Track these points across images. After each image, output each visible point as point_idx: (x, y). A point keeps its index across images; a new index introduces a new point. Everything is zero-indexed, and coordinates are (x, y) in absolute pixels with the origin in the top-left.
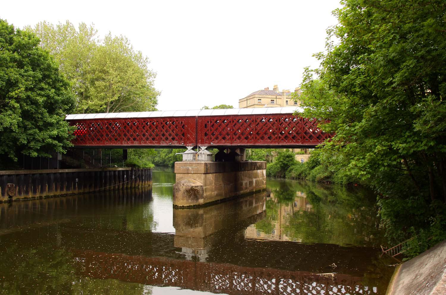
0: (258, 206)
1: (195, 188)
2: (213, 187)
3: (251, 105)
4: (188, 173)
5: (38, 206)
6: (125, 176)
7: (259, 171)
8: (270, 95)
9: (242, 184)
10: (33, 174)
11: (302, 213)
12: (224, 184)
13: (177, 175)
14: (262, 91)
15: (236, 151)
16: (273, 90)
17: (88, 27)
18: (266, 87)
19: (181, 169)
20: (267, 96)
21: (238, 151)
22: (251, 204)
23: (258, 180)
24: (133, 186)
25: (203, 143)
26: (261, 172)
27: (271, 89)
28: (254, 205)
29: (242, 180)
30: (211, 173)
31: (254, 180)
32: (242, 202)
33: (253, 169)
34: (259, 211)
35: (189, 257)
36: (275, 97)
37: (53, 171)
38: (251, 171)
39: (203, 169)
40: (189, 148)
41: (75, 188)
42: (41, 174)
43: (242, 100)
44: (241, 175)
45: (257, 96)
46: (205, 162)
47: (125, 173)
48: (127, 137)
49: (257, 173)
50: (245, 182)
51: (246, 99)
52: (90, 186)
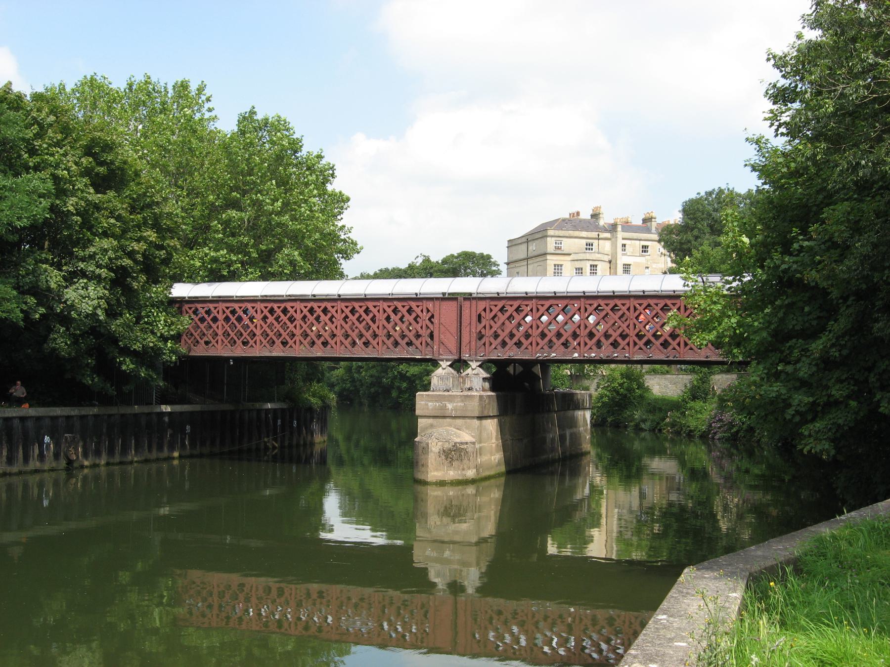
1: (462, 447)
2: (494, 445)
3: (536, 253)
4: (444, 417)
6: (295, 425)
7: (579, 413)
9: (544, 440)
10: (110, 416)
11: (694, 486)
12: (512, 440)
13: (419, 420)
14: (564, 220)
15: (533, 369)
17: (193, 87)
18: (574, 210)
19: (430, 408)
20: (577, 233)
21: (537, 370)
24: (295, 442)
27: (586, 215)
36: (595, 234)
37: (146, 409)
42: (123, 415)
45: (550, 232)
46: (478, 394)
48: (309, 338)
51: (524, 240)
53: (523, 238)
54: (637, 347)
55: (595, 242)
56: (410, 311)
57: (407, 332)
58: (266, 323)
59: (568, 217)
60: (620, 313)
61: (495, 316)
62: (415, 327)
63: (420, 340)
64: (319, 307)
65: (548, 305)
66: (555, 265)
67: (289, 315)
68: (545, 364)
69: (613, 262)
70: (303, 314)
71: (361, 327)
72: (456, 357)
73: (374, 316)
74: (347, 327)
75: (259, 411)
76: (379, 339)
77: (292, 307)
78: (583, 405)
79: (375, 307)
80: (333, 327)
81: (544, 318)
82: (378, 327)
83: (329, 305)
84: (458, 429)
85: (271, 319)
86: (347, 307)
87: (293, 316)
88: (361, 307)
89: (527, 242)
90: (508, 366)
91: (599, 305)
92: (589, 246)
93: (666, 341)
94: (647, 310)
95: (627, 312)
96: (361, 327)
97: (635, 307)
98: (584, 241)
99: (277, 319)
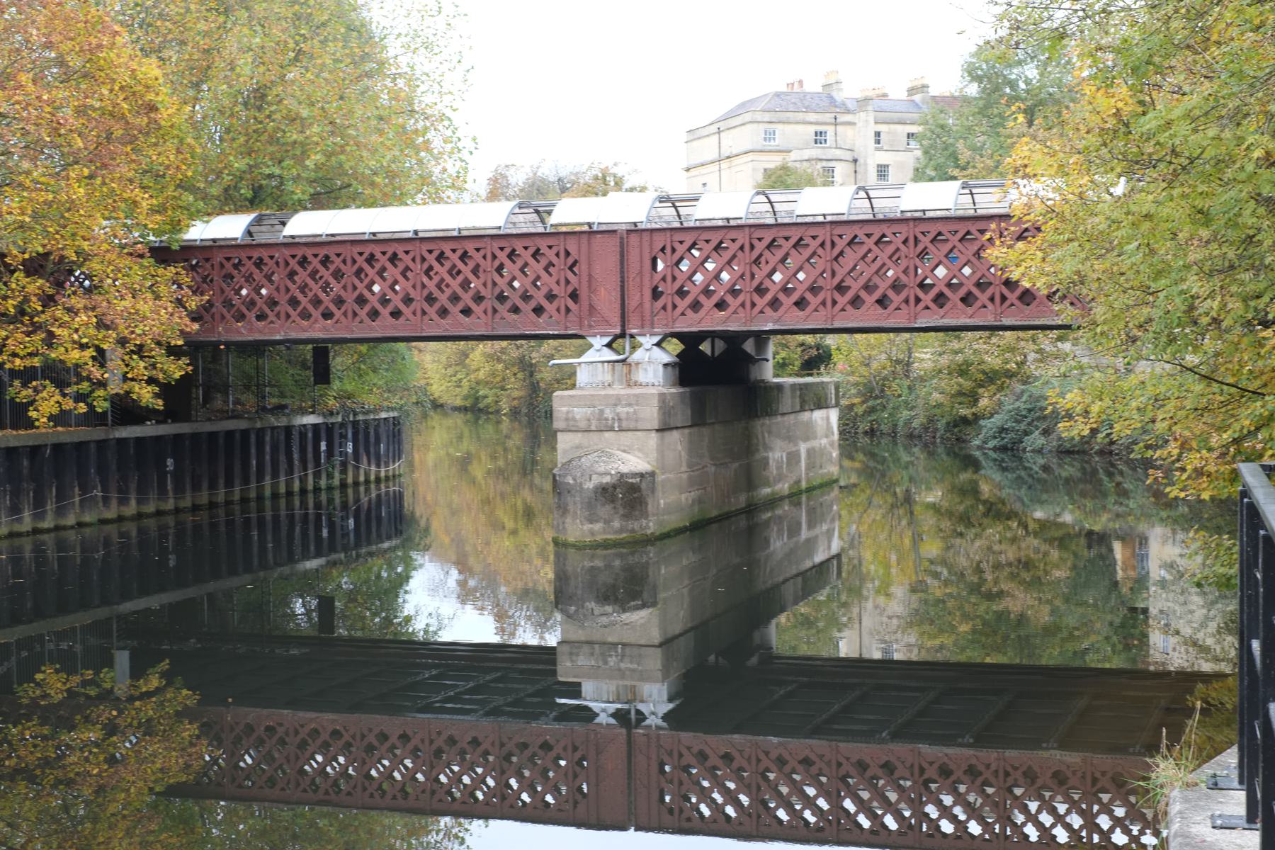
0: (816, 537)
5: (52, 554)
7: (818, 415)
8: (808, 110)
13: (560, 436)
14: (778, 95)
16: (820, 90)
20: (800, 116)
21: (749, 346)
22: (794, 530)
23: (813, 449)
25: (647, 325)
26: (822, 418)
28: (805, 534)
29: (767, 448)
30: (677, 428)
31: (803, 448)
32: (767, 523)
33: (798, 408)
34: (819, 557)
35: (603, 710)
36: (828, 117)
38: (792, 416)
39: (656, 415)
40: (598, 342)
41: (162, 491)
43: (698, 134)
44: (763, 433)
47: (323, 435)
49: (809, 425)
50: (776, 454)
51: (714, 128)
52: (142, 491)
53: (712, 127)
54: (922, 305)
55: (830, 130)
56: (536, 254)
57: (532, 291)
58: (294, 282)
59: (784, 89)
60: (891, 249)
61: (841, 254)
62: (547, 282)
63: (556, 303)
64: (316, 256)
65: (797, 238)
66: (765, 170)
67: (310, 269)
68: (761, 338)
69: (861, 161)
70: (356, 267)
71: (455, 284)
72: (618, 331)
73: (478, 266)
74: (431, 285)
75: (288, 429)
76: (487, 304)
77: (338, 255)
78: (826, 402)
79: (478, 250)
80: (409, 285)
81: (685, 266)
82: (485, 285)
83: (400, 250)
84: (624, 451)
85: (302, 276)
86: (430, 252)
87: (340, 270)
88: (526, 248)
89: (719, 131)
90: (700, 343)
91: (968, 233)
92: (819, 138)
93: (969, 293)
94: (693, 251)
95: (902, 247)
96: (455, 284)
97: (916, 238)
98: (812, 129)
99: (313, 274)
